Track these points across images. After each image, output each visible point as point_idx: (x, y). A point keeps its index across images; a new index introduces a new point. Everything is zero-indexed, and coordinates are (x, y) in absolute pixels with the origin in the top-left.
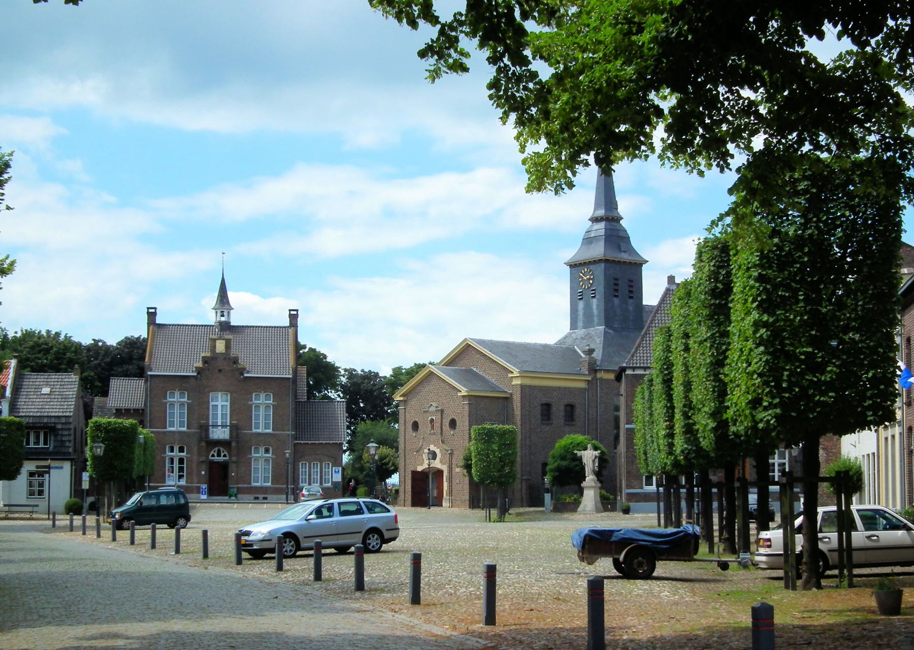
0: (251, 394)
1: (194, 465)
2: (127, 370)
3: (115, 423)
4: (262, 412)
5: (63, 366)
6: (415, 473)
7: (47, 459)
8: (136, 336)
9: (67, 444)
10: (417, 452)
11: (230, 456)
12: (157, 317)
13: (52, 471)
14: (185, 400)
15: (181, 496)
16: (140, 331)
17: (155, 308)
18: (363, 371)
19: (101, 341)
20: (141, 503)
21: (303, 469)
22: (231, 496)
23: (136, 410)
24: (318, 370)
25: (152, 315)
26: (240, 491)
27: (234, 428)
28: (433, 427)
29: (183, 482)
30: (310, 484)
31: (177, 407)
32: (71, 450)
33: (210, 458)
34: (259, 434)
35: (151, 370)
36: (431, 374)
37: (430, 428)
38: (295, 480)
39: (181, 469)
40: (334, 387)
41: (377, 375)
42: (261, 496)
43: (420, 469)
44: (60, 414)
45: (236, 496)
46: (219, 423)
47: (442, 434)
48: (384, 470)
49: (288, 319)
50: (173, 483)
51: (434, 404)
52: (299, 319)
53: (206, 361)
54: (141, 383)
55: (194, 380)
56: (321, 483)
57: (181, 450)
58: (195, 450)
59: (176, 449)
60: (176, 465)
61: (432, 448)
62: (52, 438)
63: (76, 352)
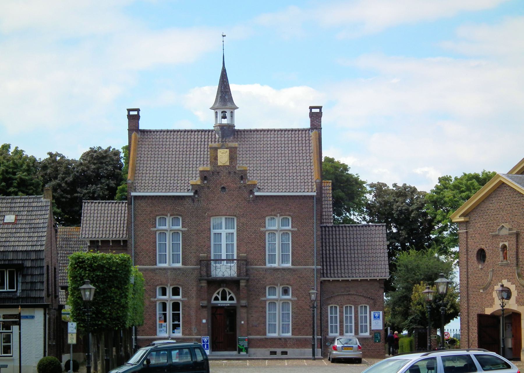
0: (264, 218)
1: (193, 313)
2: (94, 193)
3: (102, 258)
4: (169, 241)
5: (12, 189)
6: (481, 317)
7: (16, 307)
8: (105, 148)
9: (39, 286)
10: (485, 289)
11: (238, 300)
12: (140, 122)
13: (23, 321)
14: (180, 227)
15: (198, 351)
16: (116, 139)
17: (138, 110)
18: (395, 185)
19: (59, 155)
20: (148, 361)
21: (333, 314)
22: (240, 350)
23: (116, 242)
24: (342, 186)
25: (134, 119)
26: (251, 343)
27: (243, 263)
28: (505, 257)
29: (179, 334)
30: (342, 334)
31: (169, 236)
32: (44, 294)
33: (213, 302)
34: (275, 270)
35: (135, 191)
36: (502, 185)
37: (501, 258)
38: (323, 330)
39: (176, 317)
40: (358, 207)
41: (414, 190)
42: (279, 350)
43: (488, 311)
44: (30, 248)
45: (247, 350)
46: (224, 257)
47: (517, 265)
48: (441, 311)
49: (309, 120)
50: (166, 335)
51: (507, 226)
52: (323, 119)
53: (204, 176)
54: (123, 207)
55: (190, 201)
56: (356, 333)
57: (176, 292)
58: (193, 292)
59: (169, 291)
60: (169, 312)
61: (505, 283)
62: (20, 279)
63: (28, 170)
